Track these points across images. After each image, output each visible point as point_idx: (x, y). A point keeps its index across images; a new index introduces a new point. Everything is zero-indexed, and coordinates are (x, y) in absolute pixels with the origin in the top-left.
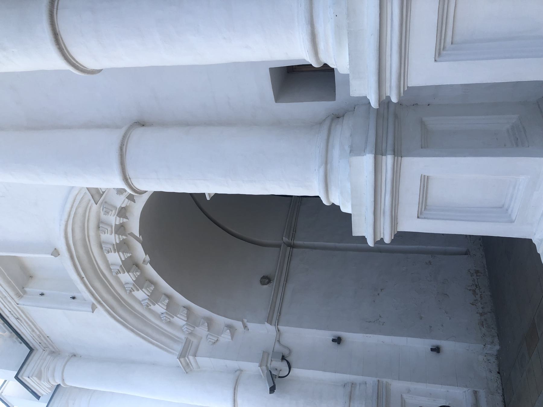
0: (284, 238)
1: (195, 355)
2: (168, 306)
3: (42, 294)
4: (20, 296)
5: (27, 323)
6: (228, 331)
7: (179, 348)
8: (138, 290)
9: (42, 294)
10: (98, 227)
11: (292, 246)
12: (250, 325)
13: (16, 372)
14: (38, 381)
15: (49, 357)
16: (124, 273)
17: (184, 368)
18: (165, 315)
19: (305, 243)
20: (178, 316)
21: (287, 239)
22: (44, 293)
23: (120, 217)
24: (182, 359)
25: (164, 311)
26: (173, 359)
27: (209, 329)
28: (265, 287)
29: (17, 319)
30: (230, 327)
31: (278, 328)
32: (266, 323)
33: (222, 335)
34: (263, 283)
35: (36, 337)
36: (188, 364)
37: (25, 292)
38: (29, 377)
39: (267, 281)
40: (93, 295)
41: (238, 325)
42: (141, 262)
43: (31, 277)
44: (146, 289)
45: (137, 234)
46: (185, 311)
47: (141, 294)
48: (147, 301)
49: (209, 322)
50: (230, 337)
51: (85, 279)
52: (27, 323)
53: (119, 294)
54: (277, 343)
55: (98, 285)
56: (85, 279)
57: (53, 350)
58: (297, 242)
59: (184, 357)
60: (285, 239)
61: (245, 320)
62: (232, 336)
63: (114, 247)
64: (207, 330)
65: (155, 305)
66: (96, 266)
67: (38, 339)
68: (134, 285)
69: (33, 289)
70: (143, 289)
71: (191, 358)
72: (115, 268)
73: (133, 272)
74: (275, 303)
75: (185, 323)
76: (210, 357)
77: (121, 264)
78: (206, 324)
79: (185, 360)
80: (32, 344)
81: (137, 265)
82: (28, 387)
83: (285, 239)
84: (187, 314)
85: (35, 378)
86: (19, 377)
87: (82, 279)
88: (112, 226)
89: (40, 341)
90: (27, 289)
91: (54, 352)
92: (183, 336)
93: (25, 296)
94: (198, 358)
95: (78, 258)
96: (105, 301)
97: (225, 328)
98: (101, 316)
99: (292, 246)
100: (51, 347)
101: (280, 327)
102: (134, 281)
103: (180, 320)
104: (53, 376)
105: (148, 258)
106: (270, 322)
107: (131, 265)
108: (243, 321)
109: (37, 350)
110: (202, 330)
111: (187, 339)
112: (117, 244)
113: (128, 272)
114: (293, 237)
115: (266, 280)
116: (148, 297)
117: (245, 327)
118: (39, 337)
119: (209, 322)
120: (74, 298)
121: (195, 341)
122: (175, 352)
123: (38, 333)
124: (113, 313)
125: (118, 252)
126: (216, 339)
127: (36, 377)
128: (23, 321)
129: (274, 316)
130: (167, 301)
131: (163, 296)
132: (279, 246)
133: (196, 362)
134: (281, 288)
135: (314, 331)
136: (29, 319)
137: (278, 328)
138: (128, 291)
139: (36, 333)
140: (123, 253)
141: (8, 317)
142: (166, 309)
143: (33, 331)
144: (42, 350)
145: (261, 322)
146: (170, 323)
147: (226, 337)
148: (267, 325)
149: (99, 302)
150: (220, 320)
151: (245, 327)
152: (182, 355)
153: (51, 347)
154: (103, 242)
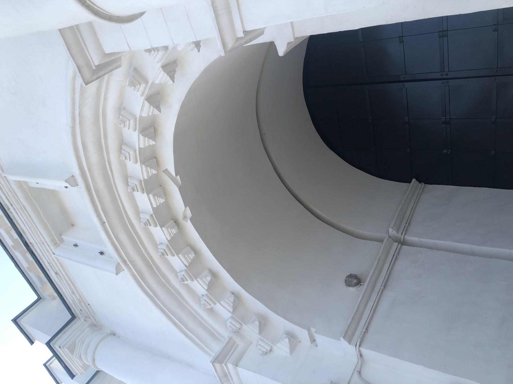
0: (390, 230)
1: (236, 365)
2: (210, 287)
3: (76, 245)
4: (56, 244)
5: (66, 281)
6: (287, 340)
7: (217, 348)
8: (173, 255)
9: (76, 245)
10: (120, 149)
11: (403, 243)
12: (319, 338)
13: (50, 338)
14: (69, 354)
15: (88, 329)
16: (156, 226)
17: (220, 379)
18: (205, 298)
19: (421, 239)
20: (222, 302)
21: (395, 232)
22: (78, 244)
23: (145, 136)
24: (217, 365)
25: (205, 292)
26: (204, 360)
27: (260, 333)
28: (352, 289)
29: (56, 273)
30: (291, 336)
31: (360, 351)
32: (342, 338)
33: (278, 345)
34: (348, 284)
35: (77, 302)
36: (226, 376)
37: (62, 241)
38: (60, 347)
39: (355, 281)
40: (117, 250)
41: (302, 334)
42: (180, 217)
43: (73, 225)
44: (184, 255)
45: (173, 172)
46: (232, 299)
47: (177, 262)
48: (183, 273)
49: (263, 324)
50: (288, 350)
51: (107, 224)
52: (66, 281)
53: (151, 257)
54: (356, 375)
55: (123, 237)
56: (107, 224)
57: (95, 323)
58: (409, 238)
59: (221, 362)
60: (392, 232)
61: (313, 330)
62: (292, 349)
63: (141, 184)
64: (258, 332)
65: (193, 280)
66: (122, 210)
67: (79, 305)
68: (167, 246)
69: (69, 238)
70: (180, 256)
71: (230, 366)
72: (145, 217)
73: (167, 228)
74: (362, 314)
75: (230, 315)
76: (255, 372)
77: (152, 212)
78: (257, 323)
79: (222, 367)
80: (75, 310)
81: (176, 222)
82: (61, 360)
83: (392, 232)
84: (234, 302)
85: (67, 350)
86: (51, 344)
87: (103, 223)
88: (135, 151)
89: (81, 308)
90: (63, 237)
91: (96, 326)
92: (226, 334)
93: (61, 245)
94: (239, 369)
95: (97, 191)
96: (132, 262)
97: (285, 336)
98: (126, 281)
99: (403, 243)
100: (92, 318)
101: (364, 350)
102: (168, 241)
103: (224, 310)
104: (86, 353)
105: (189, 213)
106: (348, 337)
107: (164, 216)
108: (309, 330)
109: (80, 318)
110: (251, 331)
111: (230, 339)
112: (145, 180)
113: (161, 226)
114: (406, 231)
115: (354, 280)
116: (185, 268)
117: (313, 340)
118: (80, 302)
119: (263, 324)
120: (102, 253)
121: (241, 344)
122: (211, 352)
123: (79, 297)
124: (140, 280)
125: (148, 194)
126: (268, 348)
127: (67, 348)
128: (63, 278)
129: (357, 331)
130: (209, 278)
131: (206, 272)
132: (381, 241)
133: (238, 374)
134: (374, 296)
135: (420, 368)
136: (69, 278)
137: (360, 351)
138: (160, 254)
139: (76, 296)
140: (154, 196)
141: (48, 270)
142: (207, 290)
143: (73, 293)
144: (83, 320)
145: (335, 337)
146: (211, 311)
147: (282, 348)
148: (344, 343)
149: (125, 262)
150: (279, 323)
151: (313, 340)
152: (219, 359)
153: (92, 318)
154: (130, 176)
